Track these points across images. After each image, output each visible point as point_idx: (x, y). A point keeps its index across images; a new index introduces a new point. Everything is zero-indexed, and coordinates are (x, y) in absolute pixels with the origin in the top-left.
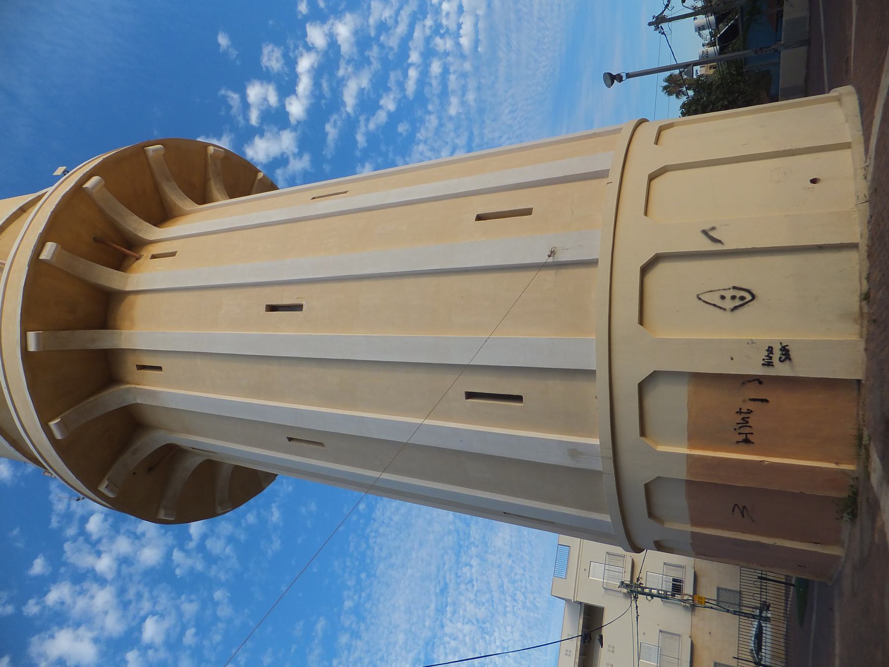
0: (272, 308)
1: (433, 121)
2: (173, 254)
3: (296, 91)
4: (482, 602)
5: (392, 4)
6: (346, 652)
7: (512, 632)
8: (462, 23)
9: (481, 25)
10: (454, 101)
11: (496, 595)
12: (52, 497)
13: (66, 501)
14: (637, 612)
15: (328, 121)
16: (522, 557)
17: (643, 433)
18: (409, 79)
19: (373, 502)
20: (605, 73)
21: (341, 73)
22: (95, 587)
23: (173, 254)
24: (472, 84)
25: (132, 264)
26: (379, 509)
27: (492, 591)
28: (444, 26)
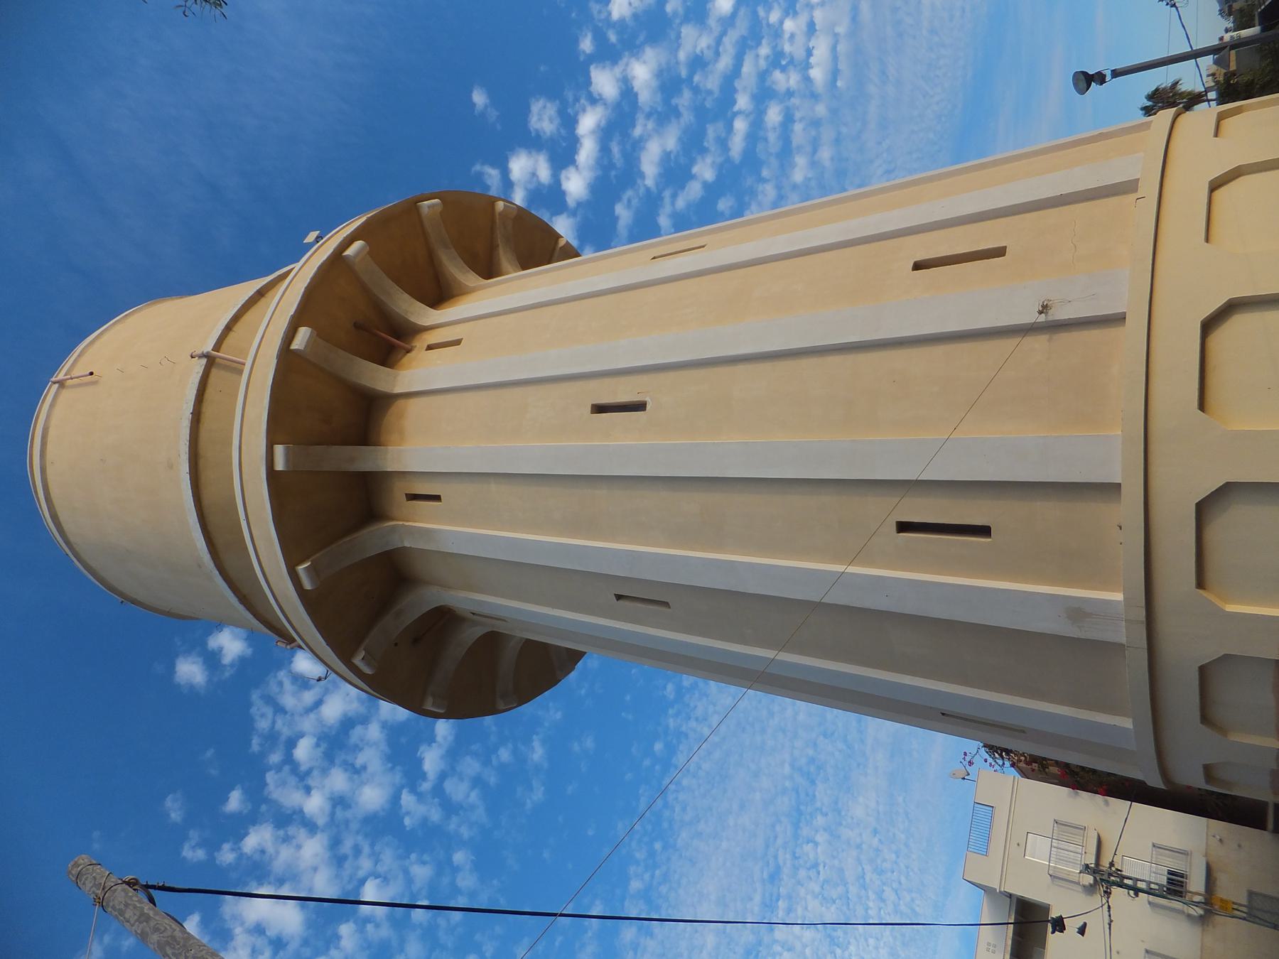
0: (599, 409)
1: (769, 191)
2: (457, 342)
4: (833, 899)
5: (711, 29)
6: (631, 953)
7: (877, 948)
8: (813, 47)
10: (801, 161)
11: (853, 890)
12: (253, 710)
14: (1110, 916)
15: (619, 199)
16: (894, 835)
17: (1200, 584)
18: (735, 134)
19: (674, 741)
20: (1077, 72)
21: (637, 132)
22: (302, 833)
23: (457, 342)
24: (827, 134)
25: (401, 358)
27: (848, 883)
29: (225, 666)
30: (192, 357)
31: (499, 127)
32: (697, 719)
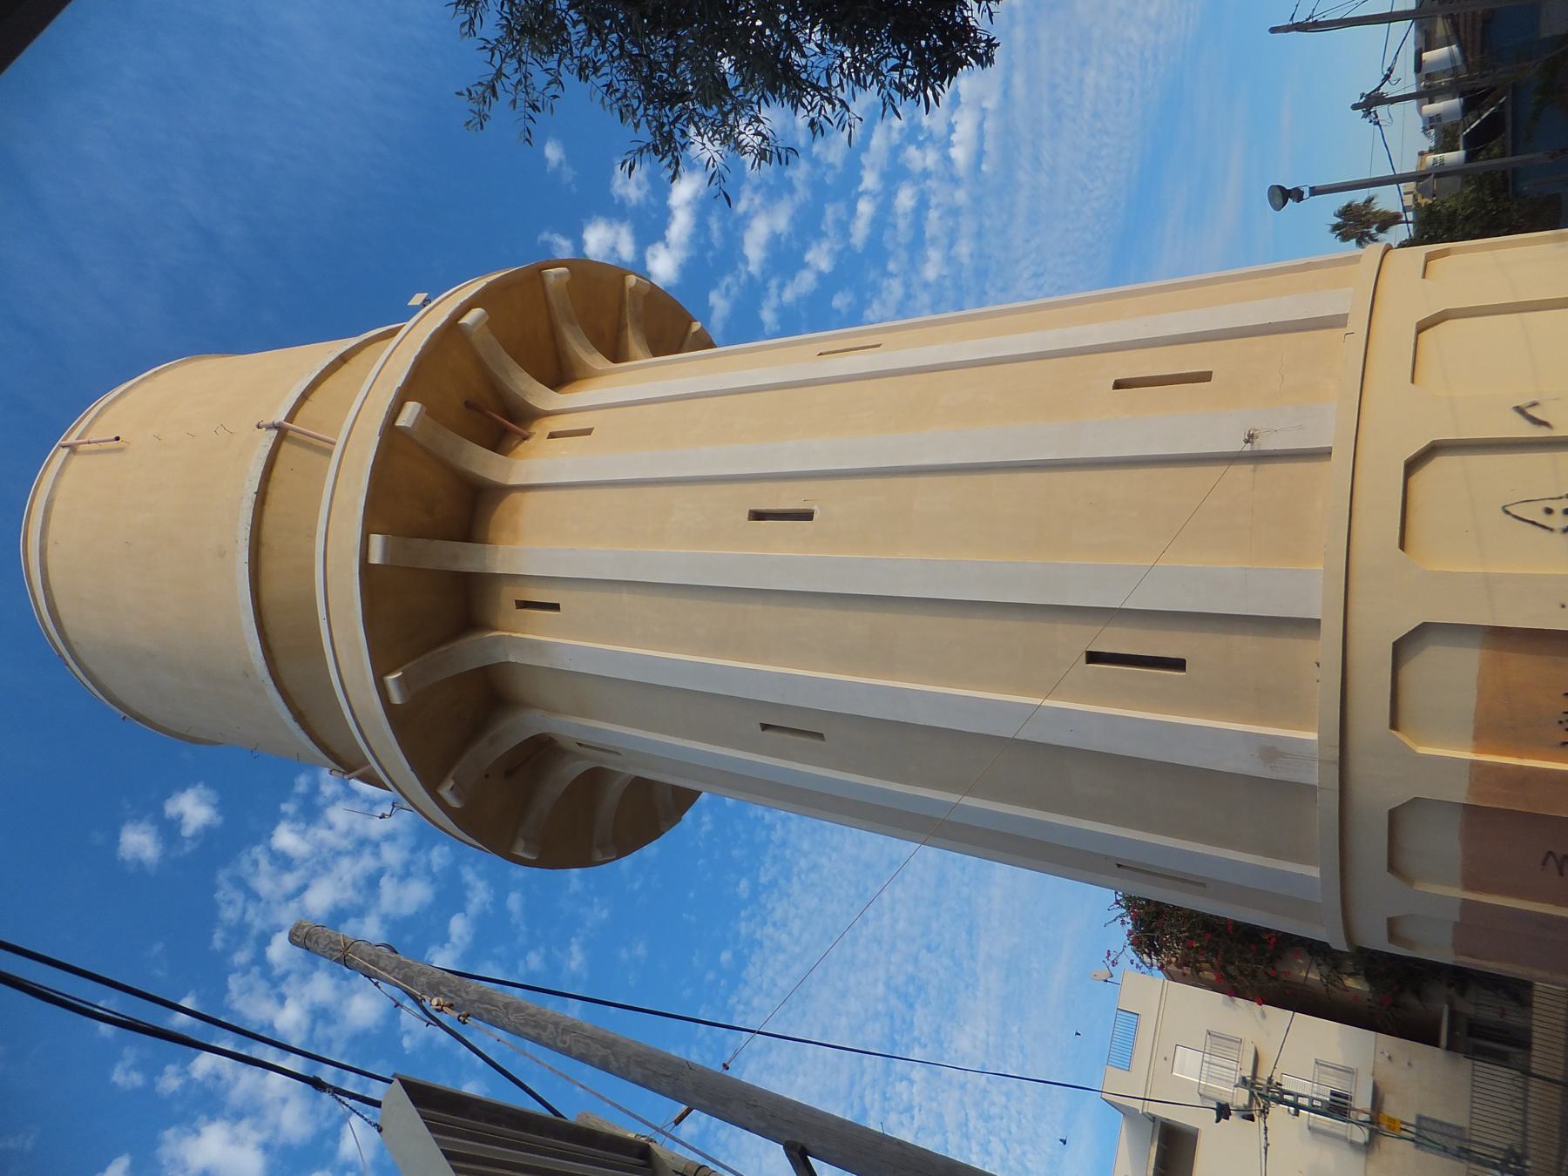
1: (895, 288)
2: (588, 432)
3: (665, 237)
8: (956, 122)
9: (989, 125)
10: (934, 255)
12: (219, 896)
13: (240, 904)
14: (1266, 1138)
15: (715, 285)
17: (1394, 725)
23: (588, 432)
24: (968, 225)
25: (517, 445)
26: (754, 964)
28: (925, 128)
29: (183, 838)
30: (259, 428)
31: (574, 189)
32: (774, 924)
